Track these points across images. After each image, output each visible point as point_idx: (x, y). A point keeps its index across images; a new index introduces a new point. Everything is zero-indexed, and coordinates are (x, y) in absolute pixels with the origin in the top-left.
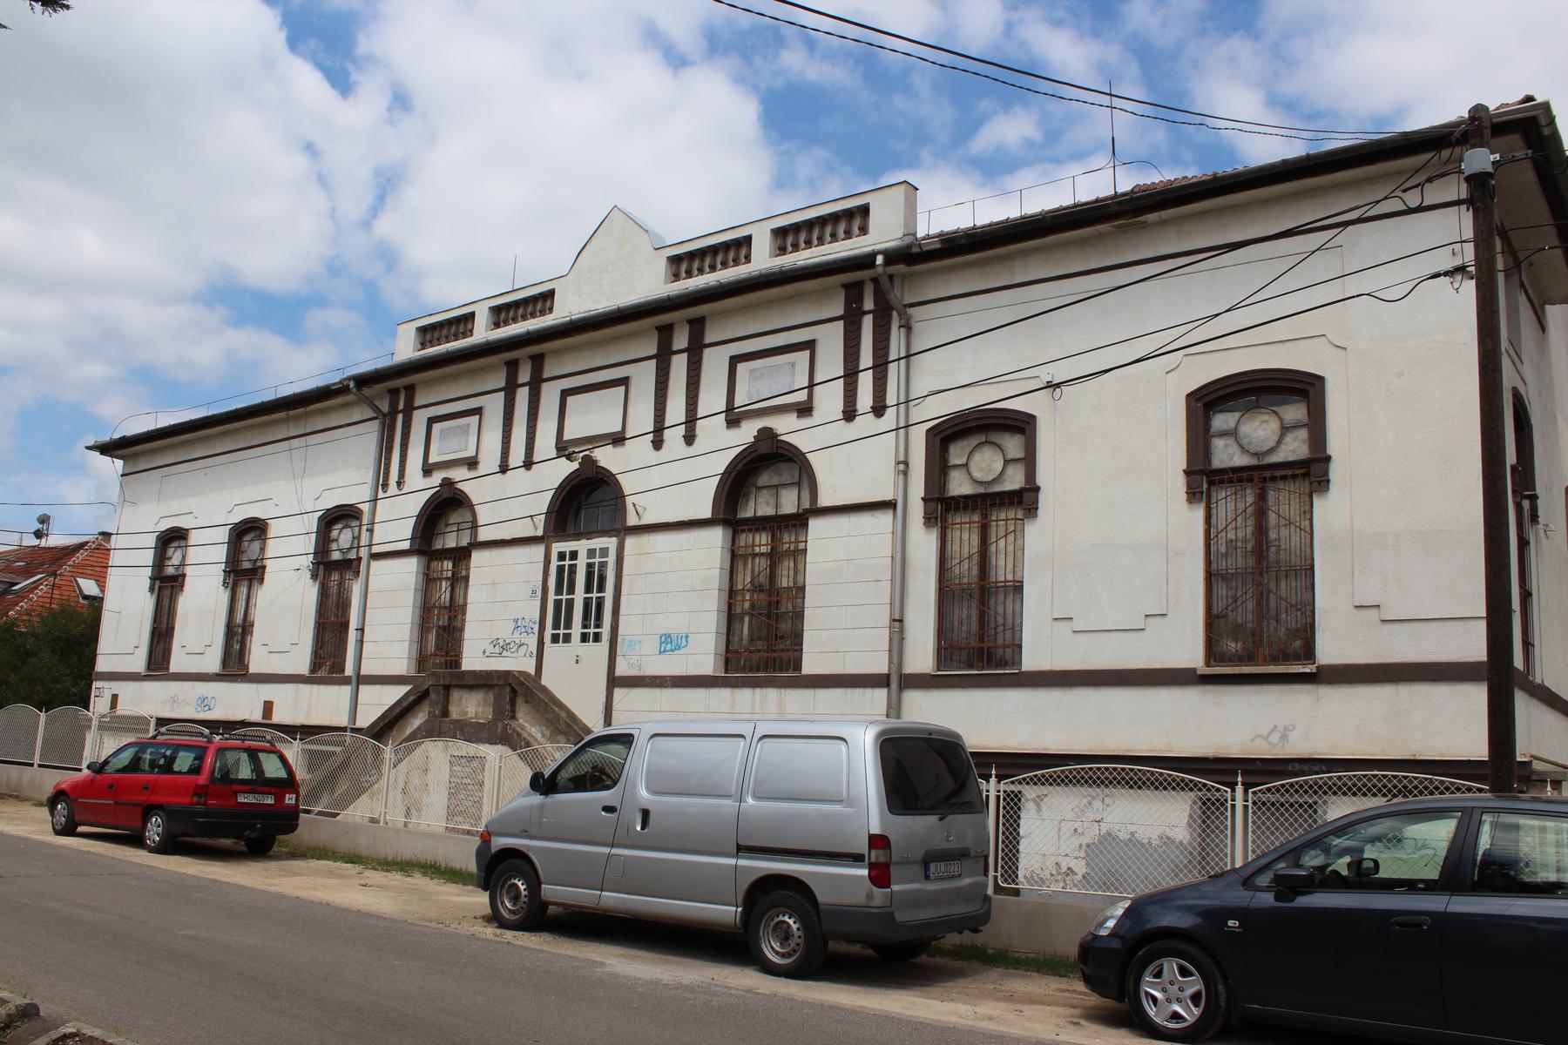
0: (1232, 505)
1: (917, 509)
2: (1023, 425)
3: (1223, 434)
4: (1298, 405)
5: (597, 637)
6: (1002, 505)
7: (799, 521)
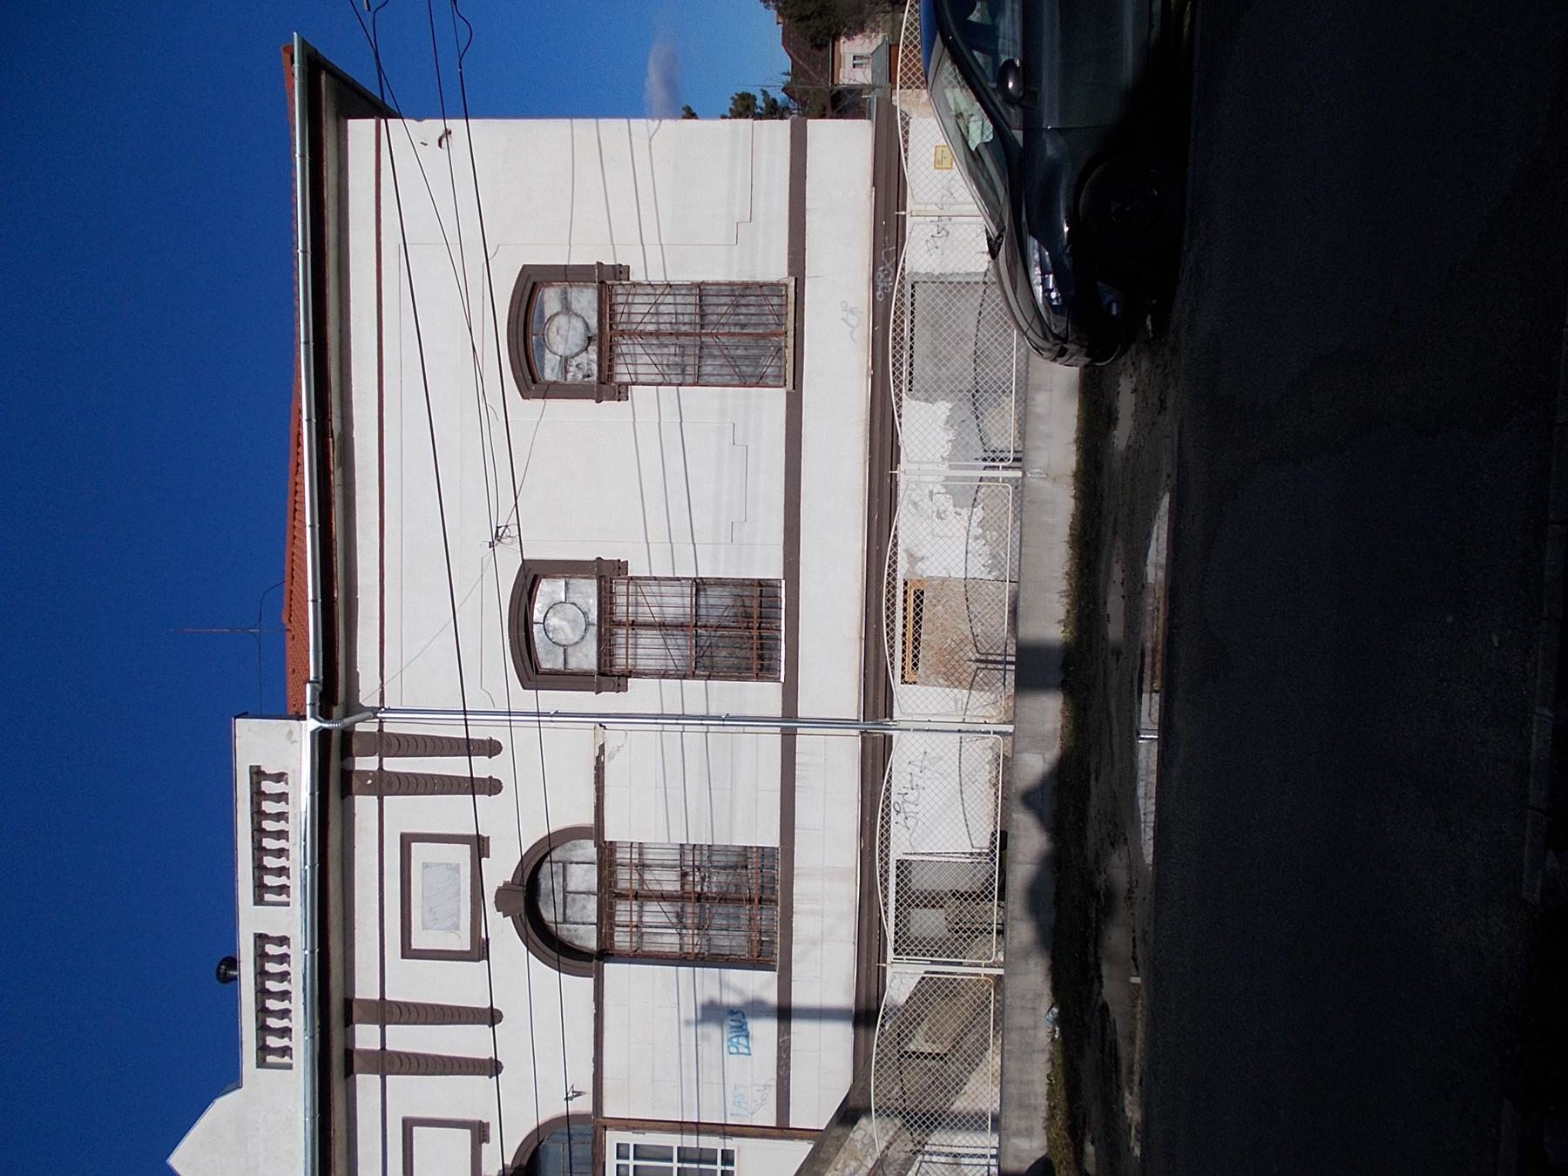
0: (634, 362)
1: (607, 701)
2: (531, 283)
4: (546, 298)
6: (611, 654)
7: (607, 855)
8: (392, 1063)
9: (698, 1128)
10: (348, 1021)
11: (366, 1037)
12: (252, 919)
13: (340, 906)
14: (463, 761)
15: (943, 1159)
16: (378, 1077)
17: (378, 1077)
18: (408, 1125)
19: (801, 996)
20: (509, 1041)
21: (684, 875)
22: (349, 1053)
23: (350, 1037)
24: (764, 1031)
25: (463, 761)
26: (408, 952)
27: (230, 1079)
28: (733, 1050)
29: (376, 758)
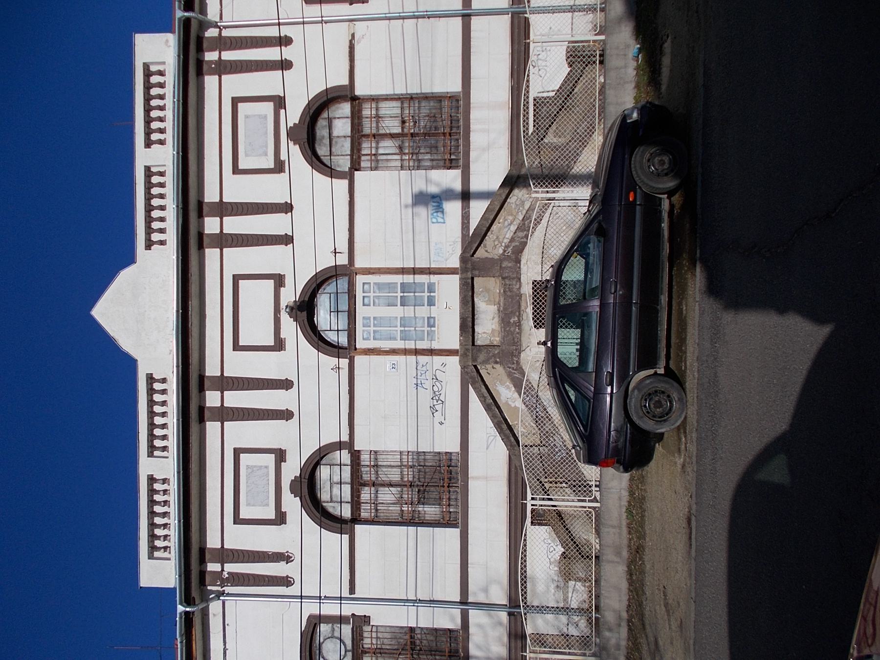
3: (333, 630)
5: (431, 288)
7: (356, 456)
8: (225, 68)
9: (414, 271)
10: (201, 215)
11: (212, 399)
12: (146, 466)
13: (195, 139)
14: (272, 49)
15: (567, 203)
16: (218, 250)
17: (218, 250)
18: (236, 278)
19: (475, 185)
20: (298, 224)
21: (403, 122)
22: (201, 235)
23: (202, 398)
24: (453, 208)
25: (272, 49)
26: (236, 170)
27: (129, 259)
28: (434, 220)
29: (217, 53)
